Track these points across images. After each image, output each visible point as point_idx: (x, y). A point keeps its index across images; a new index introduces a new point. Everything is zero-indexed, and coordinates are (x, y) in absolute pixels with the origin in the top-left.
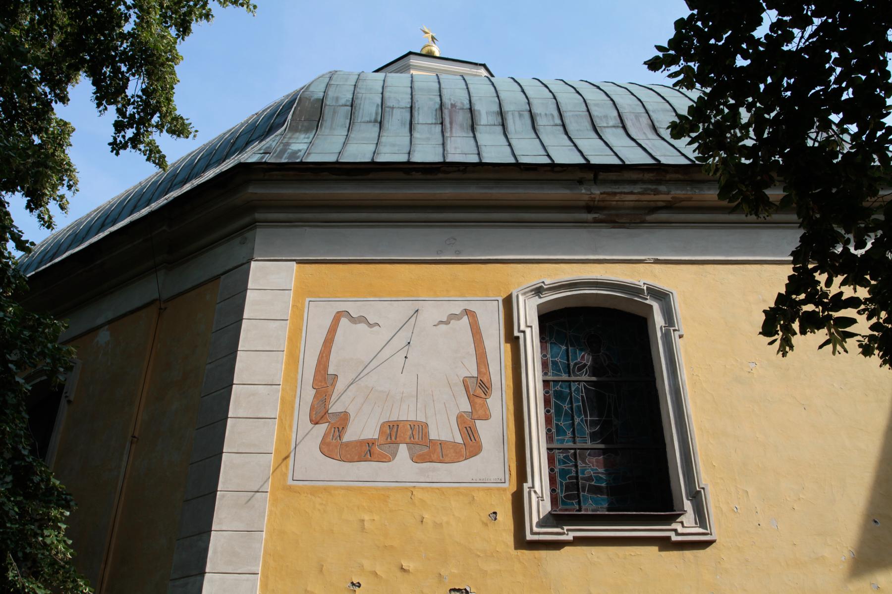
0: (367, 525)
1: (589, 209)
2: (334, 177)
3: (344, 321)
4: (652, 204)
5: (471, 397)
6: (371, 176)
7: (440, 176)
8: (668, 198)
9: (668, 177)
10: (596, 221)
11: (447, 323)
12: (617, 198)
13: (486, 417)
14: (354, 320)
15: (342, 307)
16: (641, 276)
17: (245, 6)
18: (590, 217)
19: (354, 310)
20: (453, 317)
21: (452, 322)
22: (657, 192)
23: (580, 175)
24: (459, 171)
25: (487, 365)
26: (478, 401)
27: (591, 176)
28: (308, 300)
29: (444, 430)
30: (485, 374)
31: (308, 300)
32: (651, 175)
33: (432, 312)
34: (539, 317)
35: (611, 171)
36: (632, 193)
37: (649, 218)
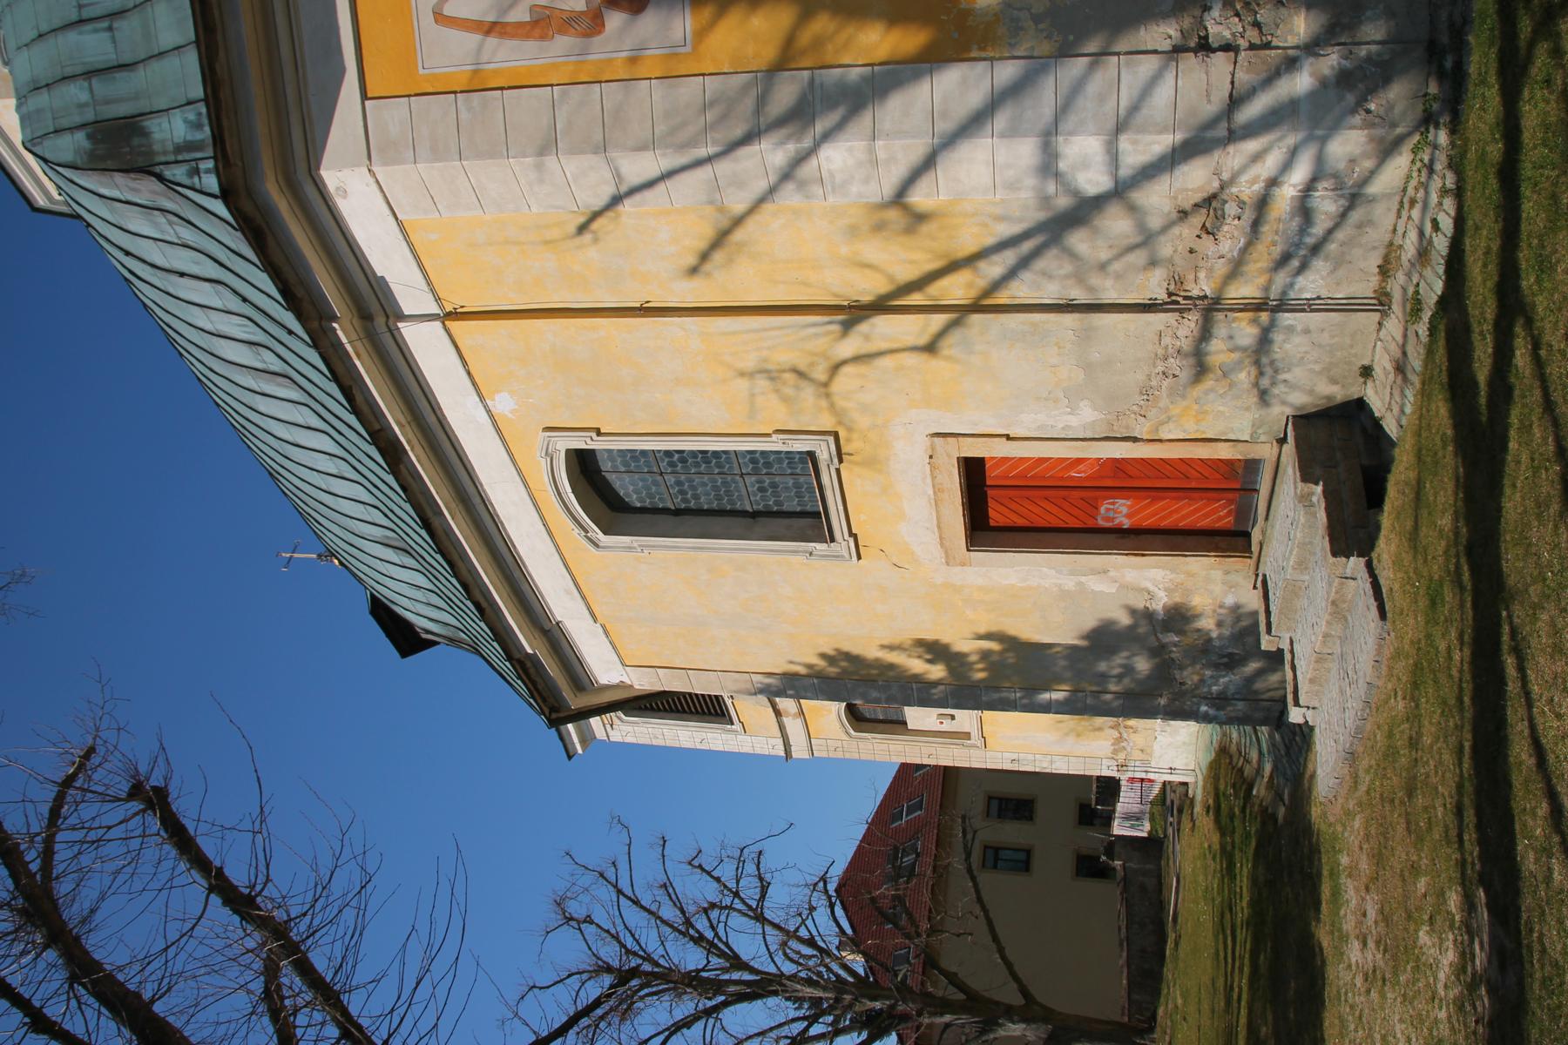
2: (222, 54)
3: (448, 10)
15: (427, 19)
28: (421, 71)
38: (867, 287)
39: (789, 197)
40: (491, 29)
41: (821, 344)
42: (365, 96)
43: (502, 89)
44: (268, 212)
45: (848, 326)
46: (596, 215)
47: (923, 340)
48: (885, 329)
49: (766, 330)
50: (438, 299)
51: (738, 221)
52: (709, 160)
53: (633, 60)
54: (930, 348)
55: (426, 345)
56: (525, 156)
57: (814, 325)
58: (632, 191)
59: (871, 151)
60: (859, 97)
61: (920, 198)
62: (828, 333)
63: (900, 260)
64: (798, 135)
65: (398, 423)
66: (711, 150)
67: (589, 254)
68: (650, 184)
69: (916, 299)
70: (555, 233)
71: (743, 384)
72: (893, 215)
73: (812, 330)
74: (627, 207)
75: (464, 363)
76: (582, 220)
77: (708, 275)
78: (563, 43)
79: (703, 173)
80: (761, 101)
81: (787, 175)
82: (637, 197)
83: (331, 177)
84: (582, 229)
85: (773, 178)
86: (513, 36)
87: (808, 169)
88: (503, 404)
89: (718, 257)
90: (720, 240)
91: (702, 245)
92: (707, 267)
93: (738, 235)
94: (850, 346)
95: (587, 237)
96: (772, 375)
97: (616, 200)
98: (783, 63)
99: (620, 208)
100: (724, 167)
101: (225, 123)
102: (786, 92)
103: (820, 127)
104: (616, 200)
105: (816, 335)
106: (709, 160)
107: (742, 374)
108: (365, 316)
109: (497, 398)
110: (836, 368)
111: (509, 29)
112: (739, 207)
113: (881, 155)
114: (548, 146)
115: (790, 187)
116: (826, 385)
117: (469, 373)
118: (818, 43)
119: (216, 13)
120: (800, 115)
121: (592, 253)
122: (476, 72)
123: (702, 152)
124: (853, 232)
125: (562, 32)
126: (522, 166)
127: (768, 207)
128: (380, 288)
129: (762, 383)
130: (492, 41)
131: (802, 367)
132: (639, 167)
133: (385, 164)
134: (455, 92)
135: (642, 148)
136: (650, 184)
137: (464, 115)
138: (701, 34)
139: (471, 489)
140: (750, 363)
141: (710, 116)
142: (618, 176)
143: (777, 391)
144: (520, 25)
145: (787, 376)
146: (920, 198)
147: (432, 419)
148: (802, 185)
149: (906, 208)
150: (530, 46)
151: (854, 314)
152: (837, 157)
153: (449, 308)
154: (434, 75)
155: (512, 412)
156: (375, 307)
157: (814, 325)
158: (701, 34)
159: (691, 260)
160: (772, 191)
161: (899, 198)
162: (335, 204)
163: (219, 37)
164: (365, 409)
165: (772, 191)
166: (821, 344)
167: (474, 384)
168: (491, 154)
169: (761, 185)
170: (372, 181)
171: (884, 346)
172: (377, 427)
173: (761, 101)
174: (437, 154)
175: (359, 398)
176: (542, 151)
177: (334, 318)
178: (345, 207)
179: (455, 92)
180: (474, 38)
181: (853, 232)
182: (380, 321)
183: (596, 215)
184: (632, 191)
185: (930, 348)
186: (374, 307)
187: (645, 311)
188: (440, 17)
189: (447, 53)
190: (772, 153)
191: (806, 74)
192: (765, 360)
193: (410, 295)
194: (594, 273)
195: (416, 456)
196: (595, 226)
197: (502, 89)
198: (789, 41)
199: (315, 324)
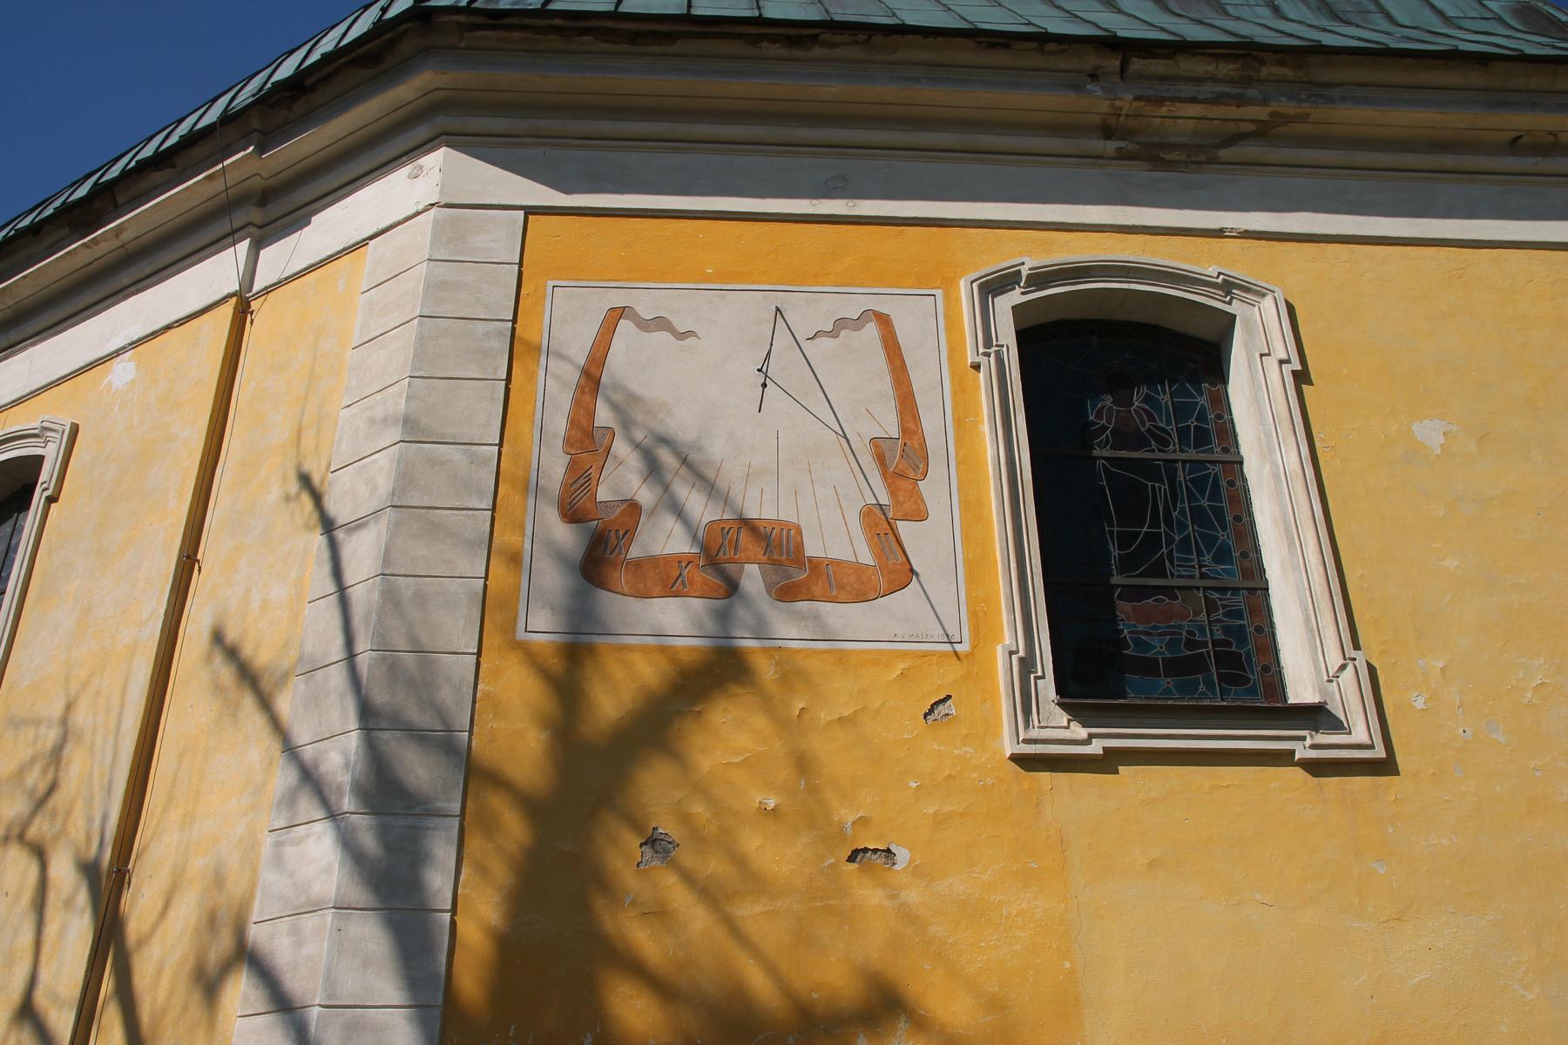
0: (846, 713)
1: (1108, 132)
2: (605, 46)
3: (625, 326)
4: (1232, 128)
5: (893, 477)
6: (678, 47)
7: (818, 51)
8: (1262, 113)
9: (1264, 72)
10: (1121, 156)
11: (833, 334)
12: (1164, 110)
13: (920, 515)
14: (644, 325)
15: (618, 299)
16: (1206, 261)
17: (32, 832)
18: (1110, 146)
19: (646, 303)
20: (841, 324)
21: (843, 333)
22: (1241, 101)
23: (1091, 61)
24: (856, 43)
25: (916, 418)
26: (904, 485)
27: (1115, 63)
28: (551, 284)
29: (834, 536)
30: (914, 433)
31: (551, 284)
32: (1232, 66)
33: (811, 310)
34: (1018, 333)
35: (1154, 56)
36: (1193, 100)
37: (1224, 153)
38: (139, 906)
39: (283, 778)
40: (591, 379)
41: (77, 828)
42: (530, 211)
43: (508, 380)
44: (400, 71)
45: (89, 870)
46: (317, 498)
47: (41, 998)
48: (74, 934)
49: (116, 742)
50: (267, 290)
51: (265, 703)
52: (351, 656)
53: (514, 559)
54: (27, 1012)
55: (217, 274)
56: (408, 398)
57: (105, 819)
58: (334, 547)
59: (315, 908)
60: (391, 885)
61: (240, 990)
62: (88, 838)
63: (161, 963)
64: (361, 792)
65: (118, 231)
66: (364, 661)
67: (276, 484)
68: (337, 573)
69: (107, 985)
70: (308, 442)
71: (56, 710)
72: (224, 943)
73: (97, 823)
74: (319, 540)
75: (181, 322)
76: (316, 480)
77: (209, 658)
78: (555, 467)
79: (336, 650)
80: (416, 734)
81: (310, 778)
82: (326, 555)
83: (437, 160)
84: (305, 480)
85: (308, 753)
86: (577, 403)
87: (308, 807)
88: (122, 372)
89: (227, 674)
90: (248, 676)
91: (247, 651)
92: (218, 659)
93: (249, 702)
94: (63, 871)
95: (294, 486)
96: (56, 755)
97: (328, 525)
98: (476, 774)
99: (319, 530)
100: (337, 677)
101: (516, 35)
102: (419, 769)
103: (363, 824)
104: (328, 525)
105: (90, 819)
106: (351, 656)
107: (69, 707)
108: (266, 196)
109: (132, 365)
110: (40, 853)
111: (587, 398)
112: (285, 704)
113: (309, 922)
114: (414, 431)
115: (290, 777)
116: (21, 837)
117: (168, 328)
118: (490, 826)
119: (655, 49)
120: (383, 790)
121: (275, 493)
122: (538, 349)
123: (363, 644)
124: (218, 880)
125: (572, 466)
126: (396, 401)
127: (275, 747)
128: (296, 219)
129: (51, 736)
130: (573, 376)
131: (57, 800)
132: (362, 556)
133: (436, 223)
134: (514, 321)
135: (387, 559)
136: (337, 573)
137: (481, 327)
138: (528, 653)
139: (29, 328)
140: (81, 717)
141: (409, 659)
142: (358, 525)
143: (33, 760)
144: (591, 414)
145: (50, 775)
146: (240, 990)
147: (125, 278)
148: (290, 800)
149: (227, 968)
150: (559, 423)
151: (108, 883)
152: (318, 858)
153: (254, 305)
154: (544, 296)
155: (110, 383)
156: (275, 209)
157: (105, 819)
158: (528, 653)
159: (231, 635)
160: (290, 750)
161: (246, 956)
162: (404, 164)
163: (624, 47)
164: (144, 184)
165: (290, 750)
166: (77, 828)
167: (154, 335)
168: (419, 355)
169: (302, 735)
170: (421, 207)
171: (51, 930)
172: (121, 199)
173: (416, 734)
174: (434, 288)
175: (158, 177)
176: (408, 422)
177: (262, 149)
178: (400, 176)
179: (514, 321)
180: (579, 351)
181: (218, 880)
182: (256, 215)
183: (317, 498)
184: (334, 547)
185: (27, 1012)
186: (275, 209)
187: (188, 562)
188: (617, 314)
189: (569, 321)
190: (340, 753)
191: (456, 807)
192: (80, 739)
193: (278, 258)
194: (252, 490)
195: (76, 253)
196: (306, 499)
197: (508, 380)
198: (498, 780)
199: (256, 124)
